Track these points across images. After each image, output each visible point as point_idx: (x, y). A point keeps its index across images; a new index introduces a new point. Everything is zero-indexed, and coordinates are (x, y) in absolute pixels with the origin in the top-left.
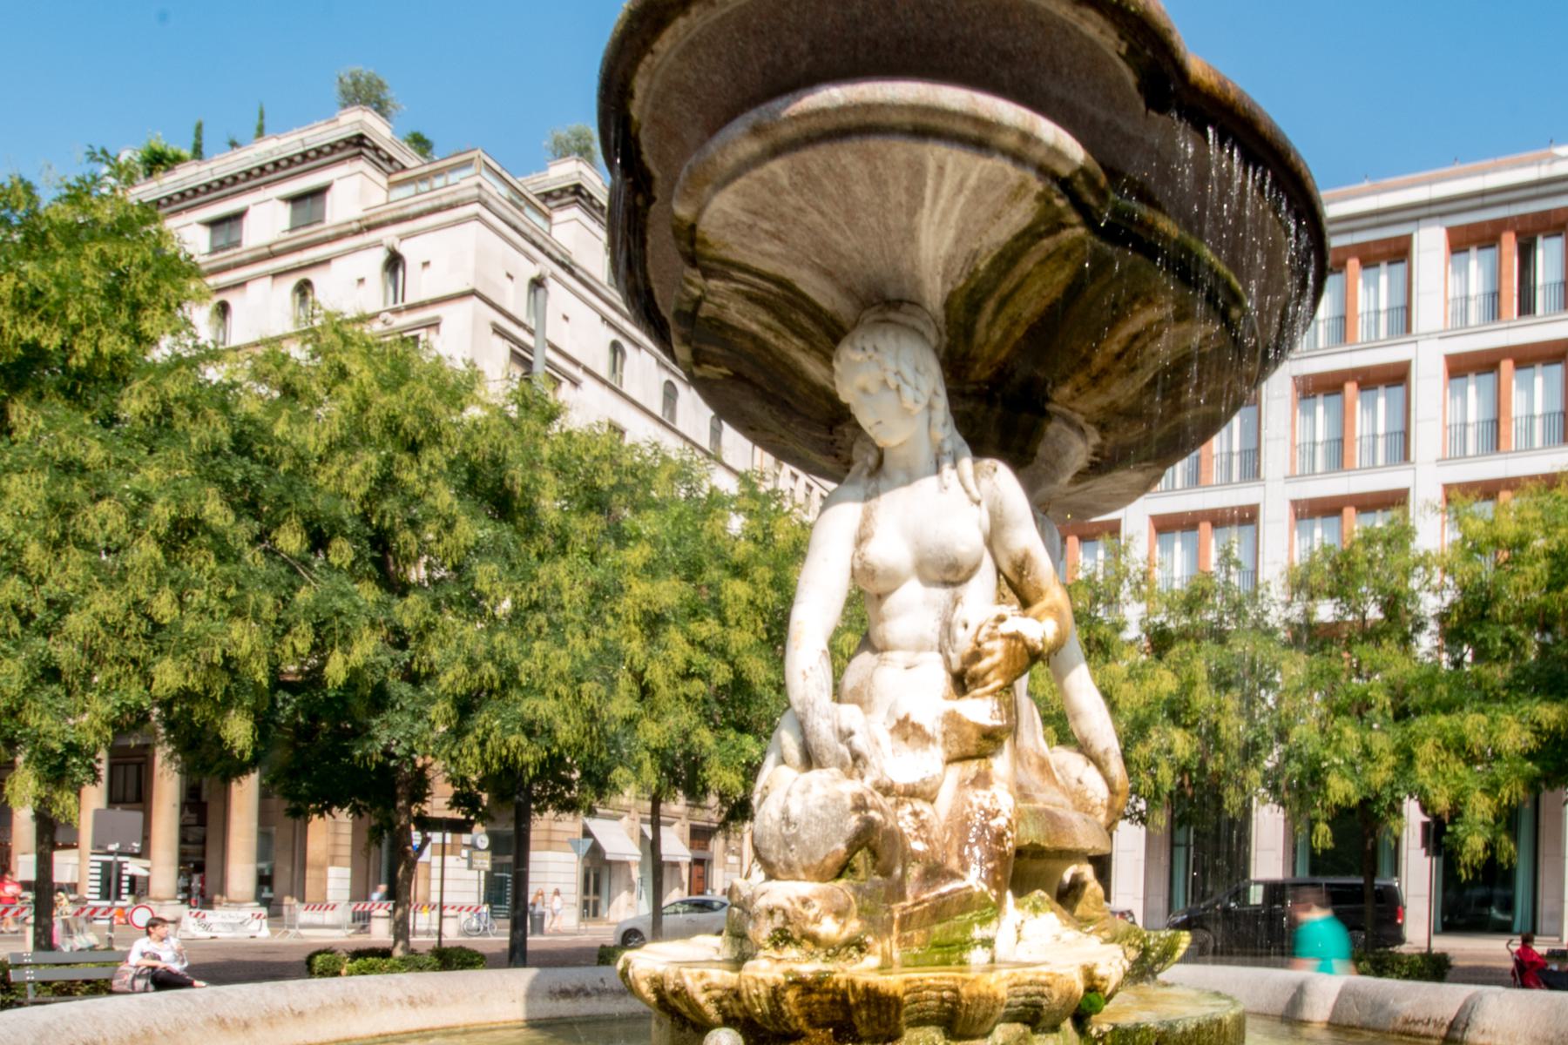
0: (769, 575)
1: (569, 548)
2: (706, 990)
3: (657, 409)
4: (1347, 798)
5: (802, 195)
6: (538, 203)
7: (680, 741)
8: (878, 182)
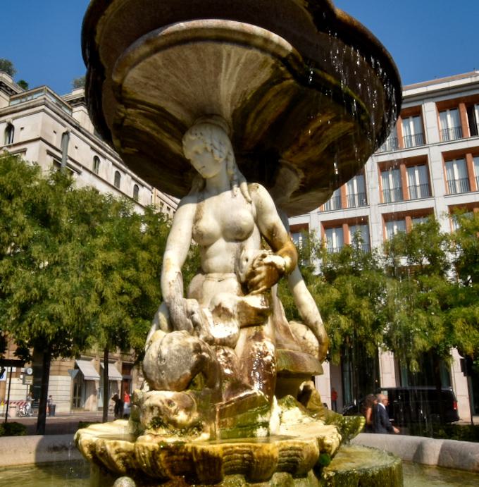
0: (157, 249)
1: (72, 238)
2: (118, 452)
3: (112, 183)
4: (424, 347)
5: (168, 69)
6: (67, 105)
7: (117, 323)
8: (201, 62)
